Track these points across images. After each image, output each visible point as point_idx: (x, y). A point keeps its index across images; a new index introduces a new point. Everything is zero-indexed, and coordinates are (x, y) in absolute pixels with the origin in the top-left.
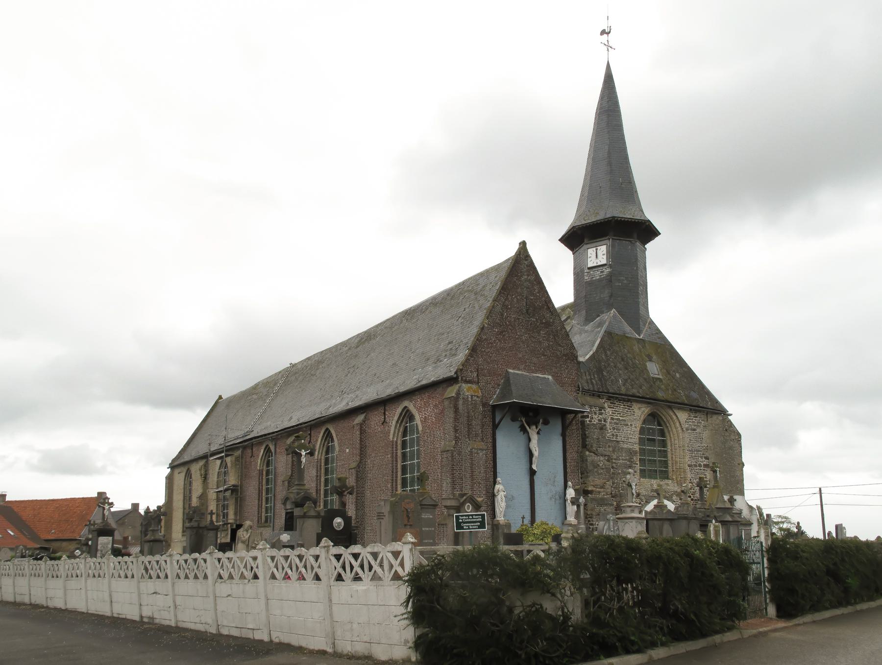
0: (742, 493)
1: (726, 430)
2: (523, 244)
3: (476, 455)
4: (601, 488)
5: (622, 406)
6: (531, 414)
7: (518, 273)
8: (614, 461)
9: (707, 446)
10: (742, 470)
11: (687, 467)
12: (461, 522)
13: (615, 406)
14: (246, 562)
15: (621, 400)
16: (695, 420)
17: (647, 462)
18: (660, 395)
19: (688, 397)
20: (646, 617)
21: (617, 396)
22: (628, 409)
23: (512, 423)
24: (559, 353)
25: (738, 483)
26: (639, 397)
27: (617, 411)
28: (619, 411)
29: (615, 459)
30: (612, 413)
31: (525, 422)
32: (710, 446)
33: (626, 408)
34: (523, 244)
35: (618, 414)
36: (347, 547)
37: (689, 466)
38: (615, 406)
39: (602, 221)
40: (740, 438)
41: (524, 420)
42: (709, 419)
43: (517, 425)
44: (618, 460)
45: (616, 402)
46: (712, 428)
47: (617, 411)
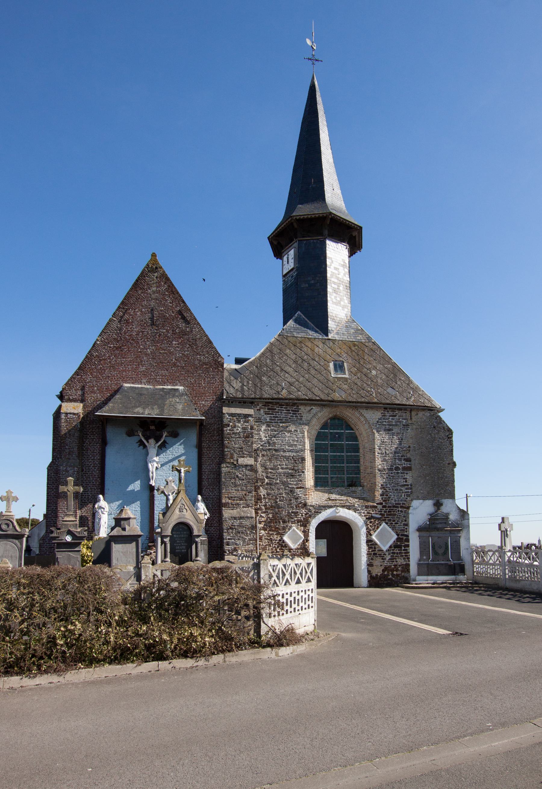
0: (452, 496)
1: (434, 427)
2: (154, 255)
3: (64, 472)
4: (241, 500)
5: (285, 412)
6: (152, 427)
7: (144, 286)
8: (270, 471)
9: (409, 447)
10: (453, 471)
11: (377, 471)
12: (175, 538)
13: (275, 412)
14: (302, 570)
15: (284, 405)
16: (392, 419)
17: (329, 470)
18: (337, 396)
19: (230, 388)
20: (157, 640)
21: (278, 401)
22: (293, 414)
23: (128, 438)
24: (197, 362)
25: (447, 486)
26: (305, 400)
27: (277, 417)
28: (280, 417)
29: (271, 469)
30: (270, 419)
31: (142, 435)
32: (414, 447)
33: (290, 413)
34: (154, 255)
35: (278, 420)
36: (279, 559)
37: (379, 470)
38: (275, 412)
39: (356, 227)
40: (452, 434)
41: (140, 435)
42: (413, 418)
43: (134, 440)
44: (275, 469)
45: (277, 407)
46: (418, 427)
47: (277, 417)
